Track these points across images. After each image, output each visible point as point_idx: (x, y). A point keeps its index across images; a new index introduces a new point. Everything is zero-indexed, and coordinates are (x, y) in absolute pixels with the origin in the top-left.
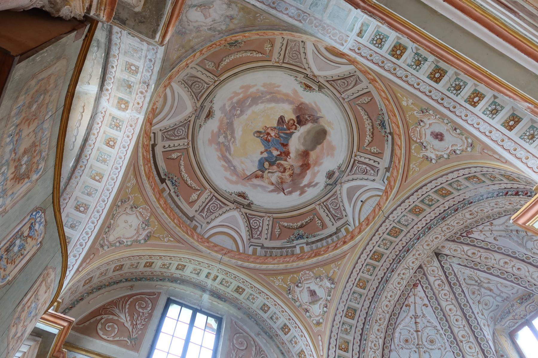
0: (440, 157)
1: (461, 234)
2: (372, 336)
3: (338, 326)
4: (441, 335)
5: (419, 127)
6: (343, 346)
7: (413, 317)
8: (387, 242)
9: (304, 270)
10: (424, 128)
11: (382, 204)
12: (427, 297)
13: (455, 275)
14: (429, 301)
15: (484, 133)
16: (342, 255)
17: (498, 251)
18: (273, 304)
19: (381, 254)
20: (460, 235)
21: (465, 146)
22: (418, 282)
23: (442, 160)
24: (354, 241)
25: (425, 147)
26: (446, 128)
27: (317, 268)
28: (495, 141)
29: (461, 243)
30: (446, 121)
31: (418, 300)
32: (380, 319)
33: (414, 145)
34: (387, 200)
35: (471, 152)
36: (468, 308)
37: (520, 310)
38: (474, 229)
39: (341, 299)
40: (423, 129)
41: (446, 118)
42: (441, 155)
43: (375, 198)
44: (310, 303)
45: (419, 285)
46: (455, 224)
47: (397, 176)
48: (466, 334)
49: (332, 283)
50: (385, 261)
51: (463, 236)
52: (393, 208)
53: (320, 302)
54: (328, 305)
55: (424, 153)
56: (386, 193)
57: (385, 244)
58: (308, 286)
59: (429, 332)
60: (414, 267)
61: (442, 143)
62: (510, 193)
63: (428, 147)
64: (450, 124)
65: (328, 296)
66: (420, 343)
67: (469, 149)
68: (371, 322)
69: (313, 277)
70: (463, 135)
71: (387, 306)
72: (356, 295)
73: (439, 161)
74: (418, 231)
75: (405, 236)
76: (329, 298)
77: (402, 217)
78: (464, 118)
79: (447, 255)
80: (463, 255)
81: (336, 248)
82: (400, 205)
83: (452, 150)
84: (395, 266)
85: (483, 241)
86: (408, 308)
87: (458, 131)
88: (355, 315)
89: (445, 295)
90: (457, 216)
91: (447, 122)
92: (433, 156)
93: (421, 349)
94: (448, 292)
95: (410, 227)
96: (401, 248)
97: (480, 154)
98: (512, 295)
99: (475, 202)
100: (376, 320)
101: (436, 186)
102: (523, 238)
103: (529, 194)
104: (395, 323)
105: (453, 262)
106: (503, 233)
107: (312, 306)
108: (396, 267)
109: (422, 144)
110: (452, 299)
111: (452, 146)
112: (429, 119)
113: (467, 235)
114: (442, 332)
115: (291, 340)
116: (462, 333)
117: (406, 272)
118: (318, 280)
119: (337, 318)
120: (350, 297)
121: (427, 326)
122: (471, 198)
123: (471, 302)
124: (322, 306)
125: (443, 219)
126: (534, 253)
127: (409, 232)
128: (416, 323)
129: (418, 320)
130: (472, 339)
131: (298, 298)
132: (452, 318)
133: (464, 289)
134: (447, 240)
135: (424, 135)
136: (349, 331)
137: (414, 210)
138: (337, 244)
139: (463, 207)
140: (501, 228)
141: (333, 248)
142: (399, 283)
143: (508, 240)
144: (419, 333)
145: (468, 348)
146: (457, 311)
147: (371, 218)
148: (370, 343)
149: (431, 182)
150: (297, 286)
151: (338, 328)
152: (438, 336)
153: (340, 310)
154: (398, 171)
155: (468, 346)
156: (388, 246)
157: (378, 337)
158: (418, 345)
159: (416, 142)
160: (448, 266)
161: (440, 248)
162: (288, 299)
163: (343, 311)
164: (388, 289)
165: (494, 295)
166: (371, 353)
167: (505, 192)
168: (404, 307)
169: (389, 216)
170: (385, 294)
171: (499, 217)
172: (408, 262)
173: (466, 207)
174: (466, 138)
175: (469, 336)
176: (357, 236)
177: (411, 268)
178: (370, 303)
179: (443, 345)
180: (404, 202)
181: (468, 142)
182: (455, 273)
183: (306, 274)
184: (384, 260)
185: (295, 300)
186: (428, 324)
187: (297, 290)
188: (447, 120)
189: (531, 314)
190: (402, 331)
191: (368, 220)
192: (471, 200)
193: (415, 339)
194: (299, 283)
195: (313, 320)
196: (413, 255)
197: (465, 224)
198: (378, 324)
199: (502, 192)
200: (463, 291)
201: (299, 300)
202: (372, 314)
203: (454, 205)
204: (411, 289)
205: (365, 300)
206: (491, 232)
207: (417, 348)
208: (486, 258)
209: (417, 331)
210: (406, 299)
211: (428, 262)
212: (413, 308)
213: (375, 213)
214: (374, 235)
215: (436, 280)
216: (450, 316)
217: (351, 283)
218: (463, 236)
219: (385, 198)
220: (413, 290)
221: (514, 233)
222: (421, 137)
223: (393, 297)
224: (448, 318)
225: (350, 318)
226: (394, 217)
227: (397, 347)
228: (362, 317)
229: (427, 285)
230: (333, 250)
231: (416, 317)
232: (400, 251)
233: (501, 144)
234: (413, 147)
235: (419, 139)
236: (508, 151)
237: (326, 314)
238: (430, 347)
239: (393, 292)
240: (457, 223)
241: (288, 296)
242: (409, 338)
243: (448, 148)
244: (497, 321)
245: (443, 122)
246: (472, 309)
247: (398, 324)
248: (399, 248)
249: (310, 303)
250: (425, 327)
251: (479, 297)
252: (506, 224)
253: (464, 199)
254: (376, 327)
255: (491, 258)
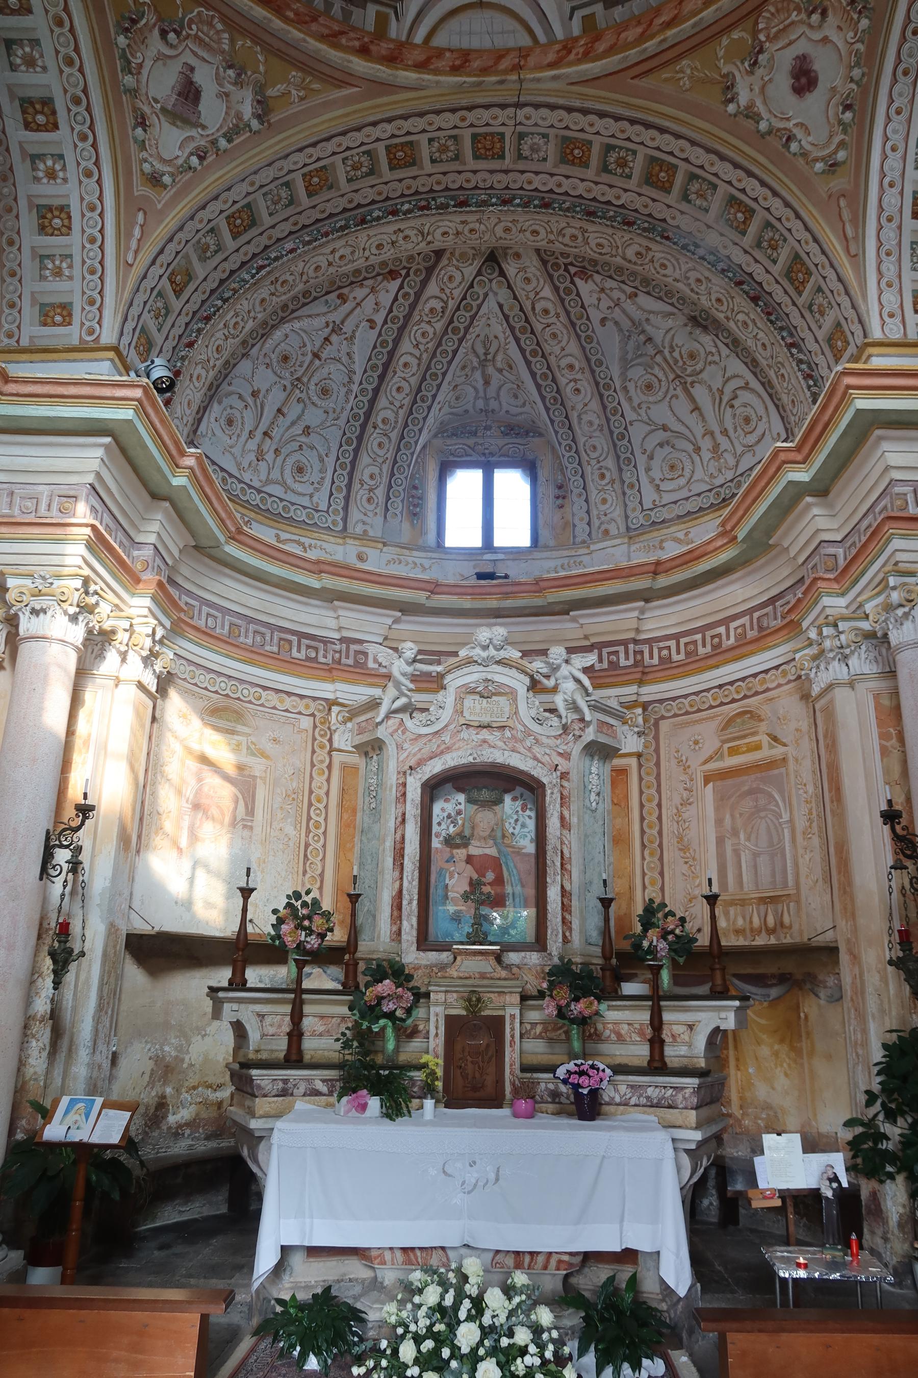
0: (751, 114)
1: (572, 264)
2: (245, 303)
3: (200, 226)
4: (350, 391)
5: (803, 16)
6: (179, 277)
7: (331, 325)
8: (452, 148)
9: (215, 9)
10: (808, 31)
11: (532, 61)
12: (391, 311)
13: (473, 318)
14: (385, 322)
15: (883, 174)
16: (337, 75)
17: (585, 340)
18: (52, 11)
19: (414, 159)
20: (566, 265)
21: (820, 154)
22: (403, 272)
23: (749, 123)
24: (389, 71)
25: (756, 63)
26: (838, 82)
27: (252, 41)
28: (881, 208)
29: (551, 277)
30: (856, 73)
31: (369, 304)
32: (284, 282)
33: (743, 34)
34: (552, 65)
35: (816, 174)
36: (435, 383)
37: (494, 441)
38: (597, 278)
39: (255, 173)
40: (803, 28)
41: (866, 70)
42: (759, 115)
43: (518, 27)
44: (163, 110)
45: (399, 281)
46: (593, 244)
47: (628, 46)
48: (393, 420)
49: (259, 117)
50: (400, 181)
51: (566, 270)
52: (552, 100)
53: (193, 132)
54: (211, 158)
55: (737, 73)
56: (565, 47)
57: (443, 149)
58: (193, 61)
59: (335, 372)
60: (436, 243)
61: (792, 98)
62: (745, 287)
63: (760, 72)
64: (854, 86)
65: (224, 136)
66: (305, 380)
67: (819, 166)
68: (263, 272)
69: (223, 52)
70: (845, 131)
71: (318, 268)
72: (284, 193)
73: (740, 119)
74: (522, 188)
75: (492, 172)
76: (223, 143)
77: (538, 134)
78: (892, 111)
79: (502, 273)
80: (528, 298)
81: (332, 38)
82: (570, 110)
83: (790, 131)
84: (406, 207)
85: (583, 306)
86: (339, 302)
87: (848, 115)
88: (245, 231)
89: (423, 334)
90: (620, 234)
91: (856, 78)
92: (743, 99)
93: (298, 391)
94: (435, 334)
95: (521, 166)
96: (456, 186)
97: (825, 196)
98: (503, 412)
99: (675, 243)
100: (277, 280)
101: (671, 153)
102: (641, 355)
103: (773, 318)
104: (293, 311)
105: (496, 294)
106: (626, 324)
107: (166, 125)
108: (409, 211)
109: (761, 51)
110: (426, 350)
111: (801, 125)
112: (840, 28)
113: (575, 274)
114: (355, 388)
115: (41, 157)
116: (389, 414)
117: (414, 239)
118: (230, 72)
119: (212, 209)
120: (272, 186)
121: (339, 361)
122: (675, 230)
123: (449, 377)
124: (191, 146)
125: (590, 214)
126: (625, 389)
127: (506, 172)
128: (326, 339)
129: (334, 338)
130: (394, 435)
131: (140, 66)
132: (396, 379)
133: (462, 351)
134: (538, 251)
135: (787, 41)
136: (209, 254)
137: (572, 146)
138: (342, 33)
139: (645, 230)
140: (637, 315)
141: (326, 31)
142: (380, 246)
143: (617, 338)
144: (317, 362)
145: (375, 444)
146: (413, 375)
147: (476, 64)
148: (232, 313)
149: (678, 136)
150: (164, 34)
151: (198, 231)
152: (343, 390)
153: (233, 195)
154: (643, 38)
155: (379, 440)
156: (444, 157)
157: (252, 314)
158: (298, 379)
159: (755, 33)
160: (481, 293)
161: (510, 252)
162: (110, 44)
163: (235, 202)
164: (351, 240)
165: (481, 394)
166: (219, 335)
167: (738, 279)
168: (333, 296)
169: (526, 105)
170: (338, 244)
171: (660, 298)
172: (440, 224)
173: (651, 235)
174: (842, 145)
175: (394, 428)
176: (407, 68)
177: (430, 238)
178: (291, 233)
179: (338, 410)
180: (585, 112)
181: (835, 152)
182: (477, 313)
183: (211, 25)
184: (401, 176)
185: (129, 62)
186: (345, 359)
187: (155, 44)
188: (863, 75)
189: (502, 459)
190: (292, 336)
191: (467, 61)
192: (670, 234)
193: (301, 366)
194: (175, 31)
195: (146, 161)
196: (463, 222)
197: (607, 257)
198: (272, 288)
199: (734, 275)
200: (455, 352)
201: (139, 73)
202: (276, 259)
203: (636, 211)
204: (378, 274)
205: (286, 220)
206: (612, 305)
207: (292, 384)
208: (554, 336)
209: (316, 356)
210: (352, 283)
211: (463, 255)
212: (350, 308)
213: (496, 63)
214: (453, 111)
215: (436, 297)
216: (395, 372)
217: (300, 158)
218: (566, 270)
219: (551, 57)
220: (380, 278)
221: (642, 338)
222: (776, 37)
223: (342, 263)
224: (390, 373)
225: (231, 231)
226: (528, 118)
227: (261, 357)
228: (252, 249)
229: (412, 292)
230: (322, 38)
231: (337, 329)
232: (447, 189)
233: (883, 221)
234: (736, 35)
235: (768, 37)
236: (880, 244)
237: (190, 174)
238: (315, 399)
239: (353, 253)
240: (599, 245)
241: (117, 34)
242: (294, 356)
243: (788, 119)
244: (444, 432)
245: (851, 68)
246: (438, 390)
247: (296, 318)
248: (454, 182)
249: (163, 110)
250: (334, 359)
251: (463, 379)
252: (651, 317)
253: (664, 220)
254: (264, 293)
255: (560, 342)
